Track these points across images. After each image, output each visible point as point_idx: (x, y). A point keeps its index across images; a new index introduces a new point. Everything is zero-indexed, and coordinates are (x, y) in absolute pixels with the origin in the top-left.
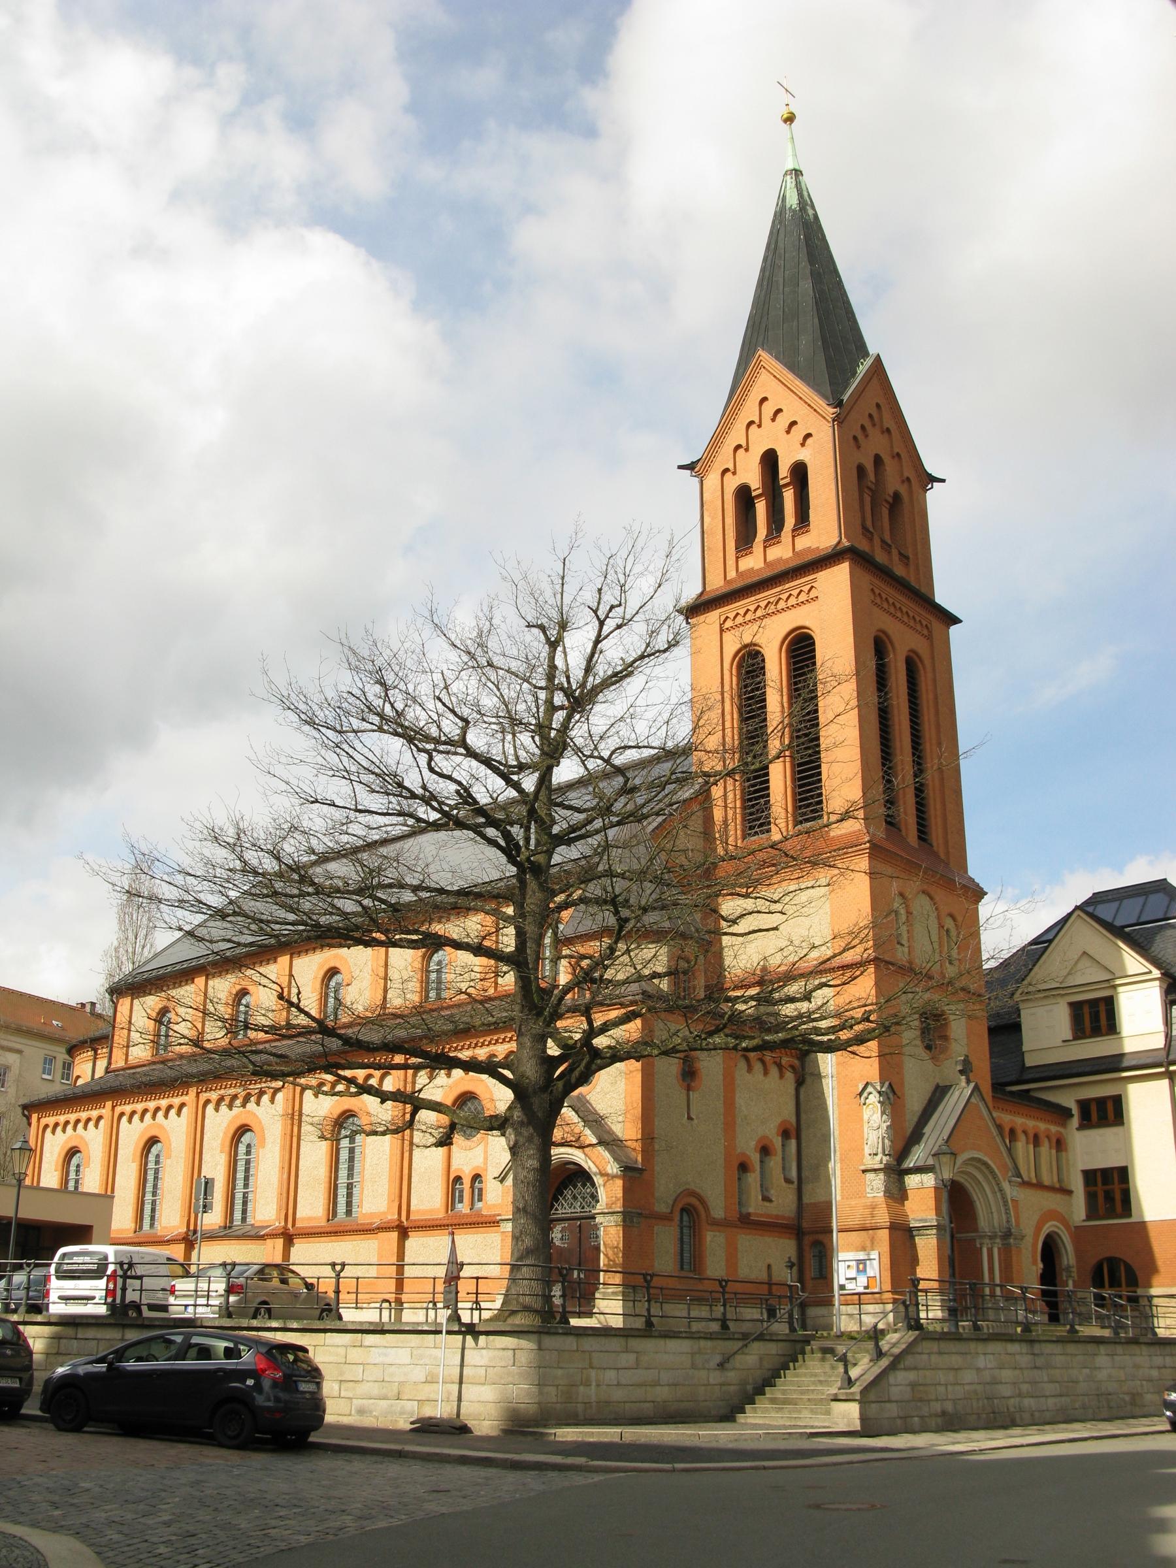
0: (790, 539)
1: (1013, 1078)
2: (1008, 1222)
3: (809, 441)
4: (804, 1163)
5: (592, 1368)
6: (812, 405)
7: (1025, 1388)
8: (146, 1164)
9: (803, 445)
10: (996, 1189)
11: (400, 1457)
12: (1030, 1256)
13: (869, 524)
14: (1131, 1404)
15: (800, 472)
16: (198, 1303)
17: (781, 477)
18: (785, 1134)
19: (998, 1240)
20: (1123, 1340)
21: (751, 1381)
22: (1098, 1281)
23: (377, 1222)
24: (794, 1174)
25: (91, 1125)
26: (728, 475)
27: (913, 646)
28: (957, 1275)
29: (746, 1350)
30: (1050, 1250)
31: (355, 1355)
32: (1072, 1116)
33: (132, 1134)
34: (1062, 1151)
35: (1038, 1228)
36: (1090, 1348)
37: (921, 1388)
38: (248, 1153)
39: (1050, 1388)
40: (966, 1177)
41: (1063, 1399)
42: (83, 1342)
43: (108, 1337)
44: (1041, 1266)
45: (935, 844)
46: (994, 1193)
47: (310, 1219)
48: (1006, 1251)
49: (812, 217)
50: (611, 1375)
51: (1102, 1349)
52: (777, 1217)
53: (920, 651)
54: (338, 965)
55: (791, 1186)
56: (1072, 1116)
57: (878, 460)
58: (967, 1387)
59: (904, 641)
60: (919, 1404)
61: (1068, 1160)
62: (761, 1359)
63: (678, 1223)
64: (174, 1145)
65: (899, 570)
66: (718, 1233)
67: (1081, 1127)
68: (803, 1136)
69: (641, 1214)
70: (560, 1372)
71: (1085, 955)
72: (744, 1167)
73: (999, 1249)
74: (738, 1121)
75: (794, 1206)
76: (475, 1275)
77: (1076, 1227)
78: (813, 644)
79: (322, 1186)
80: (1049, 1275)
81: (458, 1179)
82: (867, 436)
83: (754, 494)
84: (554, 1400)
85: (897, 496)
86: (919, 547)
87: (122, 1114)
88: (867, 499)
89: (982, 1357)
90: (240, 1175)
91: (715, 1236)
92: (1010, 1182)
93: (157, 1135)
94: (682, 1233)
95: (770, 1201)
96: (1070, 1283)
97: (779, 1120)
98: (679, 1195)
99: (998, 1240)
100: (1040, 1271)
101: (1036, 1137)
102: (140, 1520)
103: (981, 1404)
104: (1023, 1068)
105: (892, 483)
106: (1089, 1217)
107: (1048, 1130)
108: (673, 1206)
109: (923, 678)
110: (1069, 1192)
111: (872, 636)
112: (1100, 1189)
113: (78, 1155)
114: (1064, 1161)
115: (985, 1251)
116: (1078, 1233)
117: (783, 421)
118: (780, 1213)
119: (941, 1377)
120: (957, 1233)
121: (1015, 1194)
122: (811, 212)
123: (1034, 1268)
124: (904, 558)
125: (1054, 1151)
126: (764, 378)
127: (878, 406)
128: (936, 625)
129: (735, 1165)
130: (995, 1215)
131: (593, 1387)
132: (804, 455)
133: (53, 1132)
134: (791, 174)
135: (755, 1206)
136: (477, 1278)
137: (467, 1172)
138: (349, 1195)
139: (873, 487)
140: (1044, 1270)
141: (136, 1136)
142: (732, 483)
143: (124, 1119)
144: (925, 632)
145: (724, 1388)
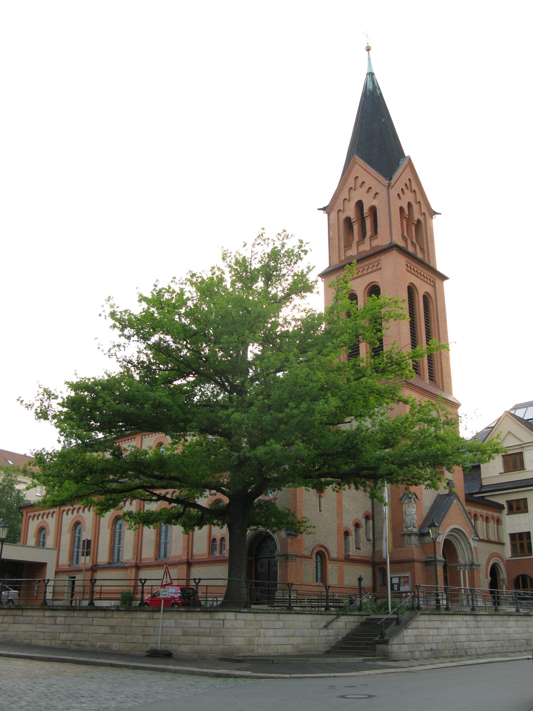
0: (369, 242)
1: (477, 491)
2: (472, 558)
3: (377, 196)
4: (376, 531)
5: (262, 628)
6: (379, 180)
7: (472, 637)
8: (75, 534)
9: (374, 198)
10: (467, 543)
11: (163, 671)
12: (485, 574)
13: (405, 234)
14: (526, 645)
15: (373, 210)
16: (205, 594)
17: (364, 213)
18: (367, 518)
19: (467, 567)
20: (521, 614)
21: (341, 635)
22: (517, 586)
23: (177, 560)
24: (371, 536)
25: (50, 516)
26: (341, 213)
27: (426, 290)
28: (449, 583)
29: (338, 620)
30: (494, 571)
31: (150, 622)
32: (504, 508)
33: (68, 520)
34: (499, 525)
35: (488, 561)
36: (506, 618)
37: (420, 637)
38: (120, 528)
39: (485, 637)
40: (452, 537)
41: (491, 642)
42: (26, 617)
43: (37, 615)
44: (490, 579)
45: (437, 381)
46: (465, 544)
47: (148, 559)
48: (472, 572)
49: (379, 94)
50: (271, 632)
51: (511, 618)
52: (363, 557)
53: (430, 293)
54: (162, 441)
55: (370, 542)
56: (504, 508)
57: (409, 204)
58: (443, 637)
59: (422, 288)
60: (419, 645)
61: (502, 529)
62: (346, 624)
63: (315, 560)
64: (87, 525)
65: (420, 255)
66: (334, 565)
67: (508, 514)
68: (375, 519)
69: (296, 555)
70: (245, 630)
71: (509, 433)
72: (347, 534)
73: (468, 571)
74: (344, 512)
75: (371, 552)
76: (151, 585)
77: (507, 560)
78: (379, 290)
79: (153, 543)
80: (494, 583)
81: (214, 540)
82: (404, 194)
83: (352, 221)
84: (243, 644)
85: (419, 221)
86: (429, 245)
87: (64, 511)
88: (405, 223)
89: (451, 622)
90: (117, 539)
91: (332, 566)
92: (473, 539)
93: (80, 520)
94: (317, 564)
95: (360, 549)
96: (504, 587)
97: (364, 511)
98: (315, 547)
99: (467, 567)
100: (489, 581)
101: (487, 518)
102: (10, 706)
103: (450, 645)
104: (482, 486)
105: (417, 216)
106: (512, 556)
107: (492, 515)
108: (312, 552)
109: (431, 305)
110: (503, 544)
111: (407, 286)
112: (518, 542)
113: (44, 530)
114: (501, 529)
115: (461, 572)
116: (508, 563)
117: (365, 187)
118: (364, 555)
119: (431, 632)
120: (449, 563)
121: (476, 545)
122: (378, 92)
123: (487, 579)
124: (422, 249)
125: (496, 525)
126: (357, 167)
127: (409, 179)
128: (437, 281)
129: (343, 532)
130: (466, 555)
131: (262, 638)
132: (375, 203)
133: (33, 519)
134: (369, 74)
135: (353, 552)
136: (207, 586)
137: (218, 536)
138: (166, 548)
139: (407, 217)
140: (491, 580)
141: (70, 521)
142: (343, 216)
143: (65, 513)
144: (432, 284)
145: (327, 638)
